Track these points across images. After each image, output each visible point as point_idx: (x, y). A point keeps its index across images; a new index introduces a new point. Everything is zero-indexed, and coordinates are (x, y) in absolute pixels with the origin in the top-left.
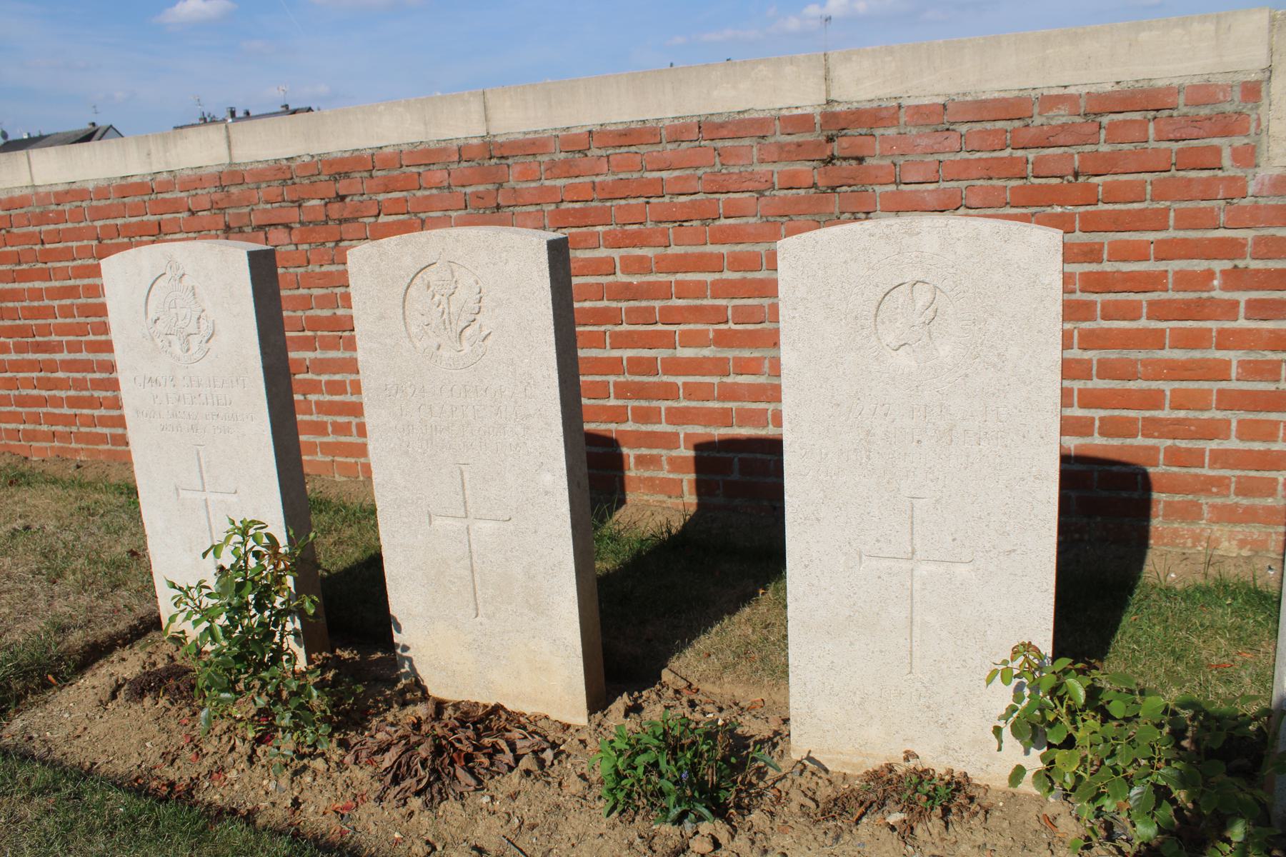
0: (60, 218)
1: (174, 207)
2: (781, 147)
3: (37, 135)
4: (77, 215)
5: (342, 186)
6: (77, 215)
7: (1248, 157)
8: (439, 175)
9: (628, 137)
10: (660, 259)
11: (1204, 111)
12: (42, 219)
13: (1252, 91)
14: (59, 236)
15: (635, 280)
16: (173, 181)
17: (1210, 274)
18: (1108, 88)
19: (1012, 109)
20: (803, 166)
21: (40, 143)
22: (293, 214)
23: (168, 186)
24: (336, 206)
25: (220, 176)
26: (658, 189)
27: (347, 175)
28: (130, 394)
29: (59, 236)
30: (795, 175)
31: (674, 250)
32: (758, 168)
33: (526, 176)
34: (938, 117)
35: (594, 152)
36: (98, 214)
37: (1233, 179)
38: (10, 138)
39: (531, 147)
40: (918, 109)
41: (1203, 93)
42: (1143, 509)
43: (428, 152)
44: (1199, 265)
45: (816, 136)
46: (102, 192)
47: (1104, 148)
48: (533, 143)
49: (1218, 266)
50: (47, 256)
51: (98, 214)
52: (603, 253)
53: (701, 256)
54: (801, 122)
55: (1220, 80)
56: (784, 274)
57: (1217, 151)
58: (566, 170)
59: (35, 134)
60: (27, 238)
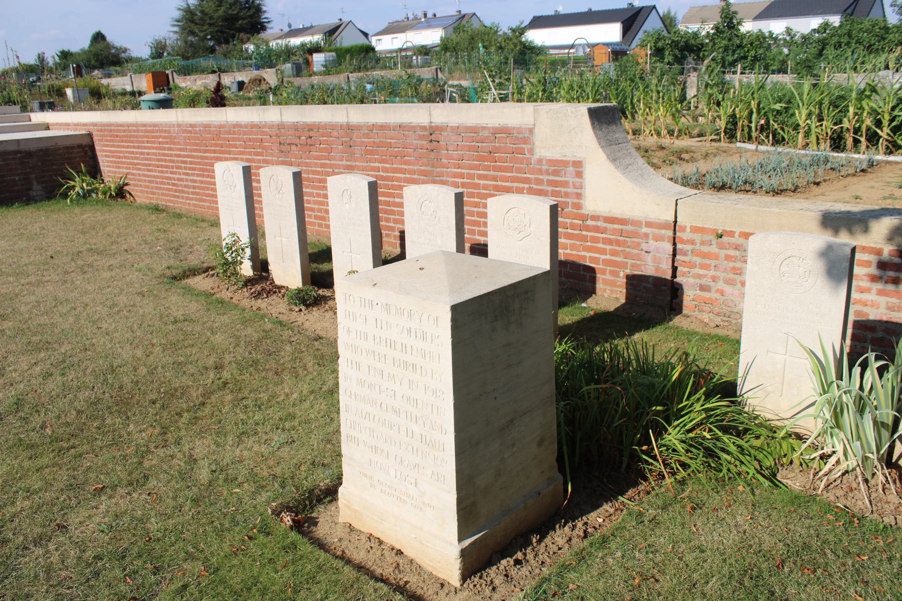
0: (234, 133)
1: (265, 133)
2: (419, 135)
3: (309, 25)
4: (239, 133)
5: (311, 134)
6: (239, 133)
7: (531, 151)
8: (336, 134)
9: (383, 127)
10: (391, 168)
11: (521, 136)
12: (229, 133)
13: (531, 131)
14: (234, 139)
15: (385, 174)
16: (266, 125)
17: (524, 188)
18: (497, 126)
19: (474, 130)
20: (425, 142)
21: (309, 31)
22: (297, 141)
23: (264, 126)
24: (309, 140)
25: (278, 125)
26: (390, 145)
27: (312, 130)
28: (220, 199)
29: (234, 139)
30: (423, 145)
31: (394, 166)
32: (415, 142)
33: (358, 137)
34: (457, 130)
35: (375, 131)
36: (245, 133)
37: (528, 158)
38: (293, 28)
39: (358, 127)
40: (452, 127)
41: (520, 130)
42: (593, 280)
43: (333, 125)
44: (521, 185)
45: (427, 133)
46: (246, 126)
47: (497, 145)
48: (359, 126)
49: (526, 186)
50: (230, 146)
51: (245, 133)
52: (377, 165)
53: (401, 169)
54: (423, 128)
55: (523, 126)
56: (328, 185)
57: (524, 149)
58: (367, 136)
59: (308, 25)
60: (225, 139)
